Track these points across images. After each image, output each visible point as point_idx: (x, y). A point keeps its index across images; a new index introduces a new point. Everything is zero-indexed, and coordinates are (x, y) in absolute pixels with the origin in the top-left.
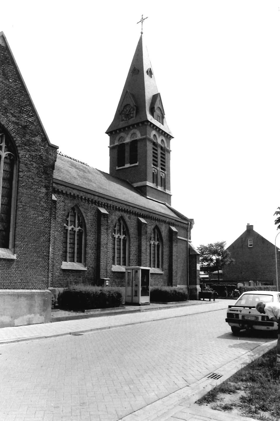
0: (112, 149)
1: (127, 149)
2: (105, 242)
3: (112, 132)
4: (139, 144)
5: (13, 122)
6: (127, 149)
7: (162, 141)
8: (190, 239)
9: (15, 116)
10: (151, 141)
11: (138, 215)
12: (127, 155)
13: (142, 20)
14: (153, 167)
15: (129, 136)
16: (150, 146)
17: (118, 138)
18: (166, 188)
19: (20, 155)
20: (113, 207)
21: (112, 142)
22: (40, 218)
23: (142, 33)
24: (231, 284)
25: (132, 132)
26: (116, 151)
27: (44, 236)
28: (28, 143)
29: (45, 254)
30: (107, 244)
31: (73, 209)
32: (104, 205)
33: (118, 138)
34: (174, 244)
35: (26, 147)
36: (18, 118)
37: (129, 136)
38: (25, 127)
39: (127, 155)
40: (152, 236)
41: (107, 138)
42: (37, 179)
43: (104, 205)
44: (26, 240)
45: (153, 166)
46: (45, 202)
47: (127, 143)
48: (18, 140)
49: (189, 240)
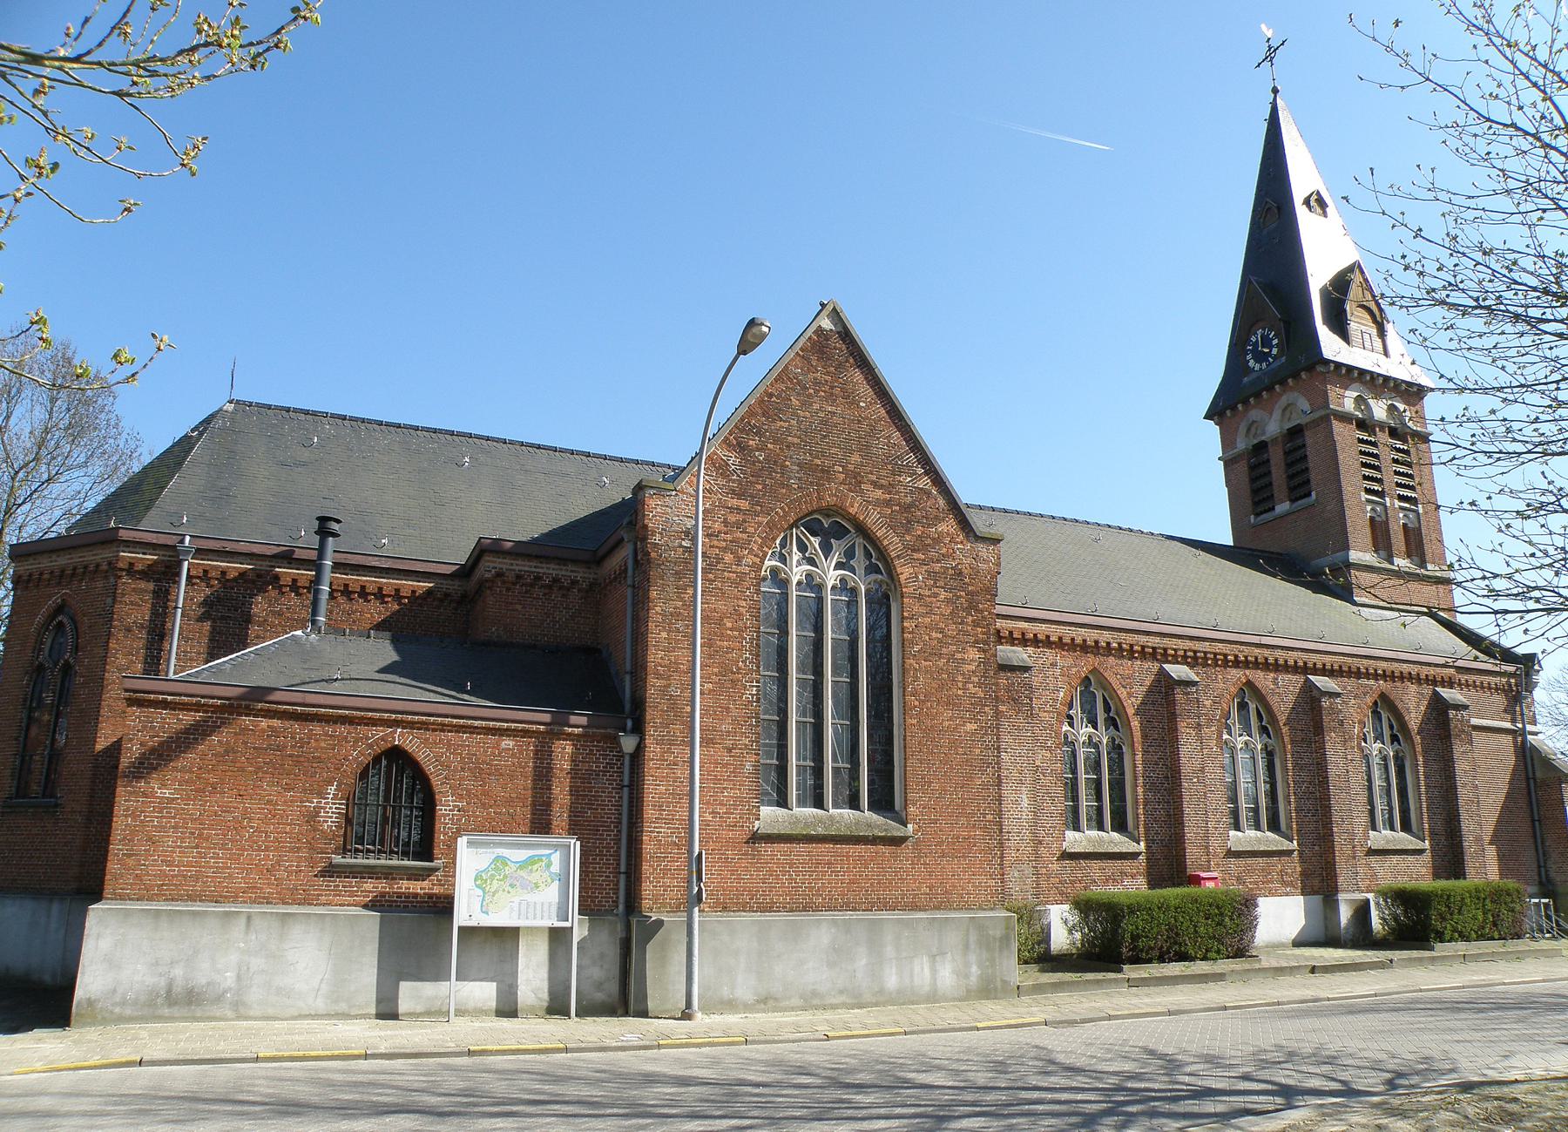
0: (1229, 463)
1: (1276, 457)
2: (1197, 764)
3: (1226, 407)
4: (1309, 439)
5: (878, 503)
6: (1276, 457)
7: (1392, 408)
8: (1534, 723)
9: (881, 487)
10: (1345, 418)
11: (1305, 670)
12: (1278, 474)
13: (1271, 54)
14: (1368, 501)
15: (1277, 414)
16: (1345, 435)
17: (1242, 429)
18: (1428, 557)
19: (902, 578)
20: (1215, 660)
21: (1227, 442)
22: (970, 727)
23: (1275, 91)
24: (1135, 778)
25: (1284, 400)
26: (1242, 467)
27: (983, 772)
28: (920, 545)
29: (989, 817)
30: (1202, 770)
31: (1086, 681)
32: (1185, 657)
33: (1242, 429)
34: (1458, 749)
35: (916, 556)
36: (889, 488)
37: (1277, 414)
38: (907, 508)
39: (1278, 474)
40: (1369, 728)
41: (1213, 430)
42: (952, 630)
43: (1185, 657)
44: (935, 786)
45: (1364, 496)
46: (980, 685)
47: (1274, 440)
48: (893, 543)
49: (1529, 728)
